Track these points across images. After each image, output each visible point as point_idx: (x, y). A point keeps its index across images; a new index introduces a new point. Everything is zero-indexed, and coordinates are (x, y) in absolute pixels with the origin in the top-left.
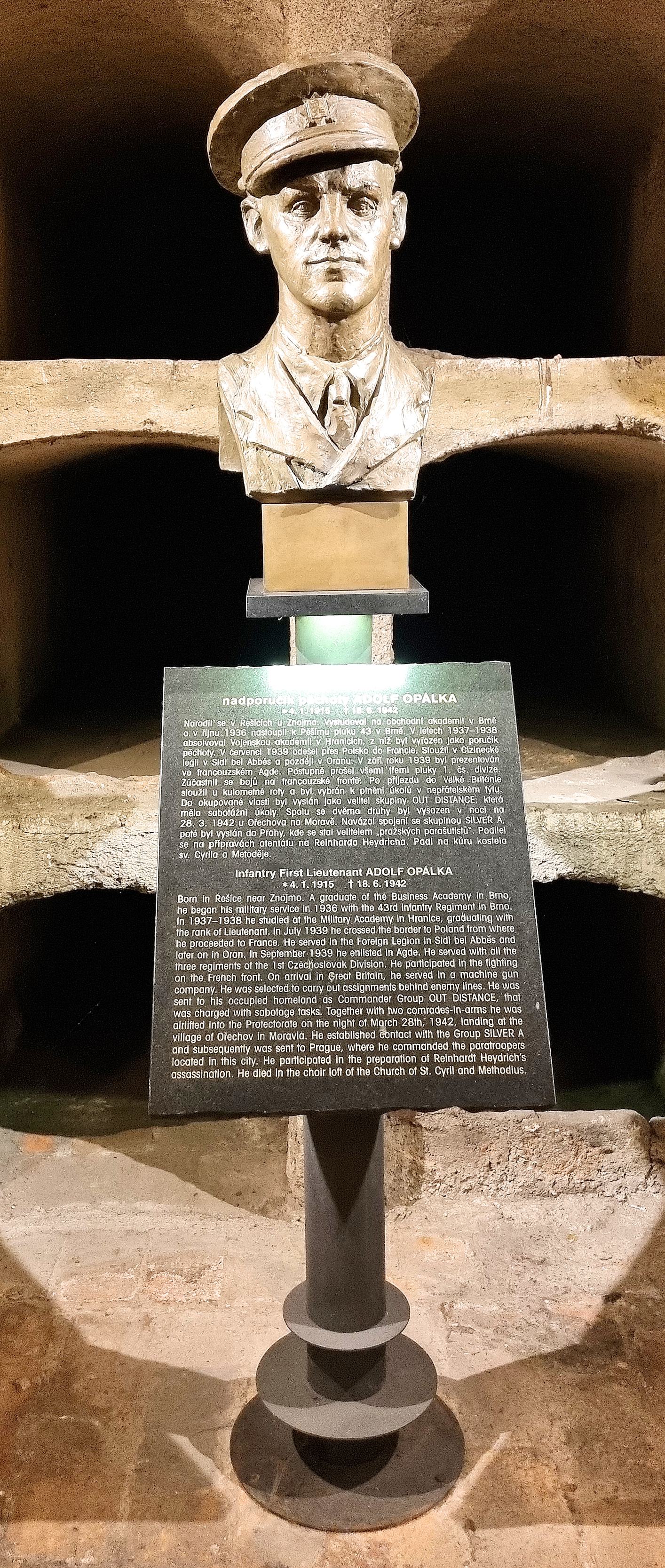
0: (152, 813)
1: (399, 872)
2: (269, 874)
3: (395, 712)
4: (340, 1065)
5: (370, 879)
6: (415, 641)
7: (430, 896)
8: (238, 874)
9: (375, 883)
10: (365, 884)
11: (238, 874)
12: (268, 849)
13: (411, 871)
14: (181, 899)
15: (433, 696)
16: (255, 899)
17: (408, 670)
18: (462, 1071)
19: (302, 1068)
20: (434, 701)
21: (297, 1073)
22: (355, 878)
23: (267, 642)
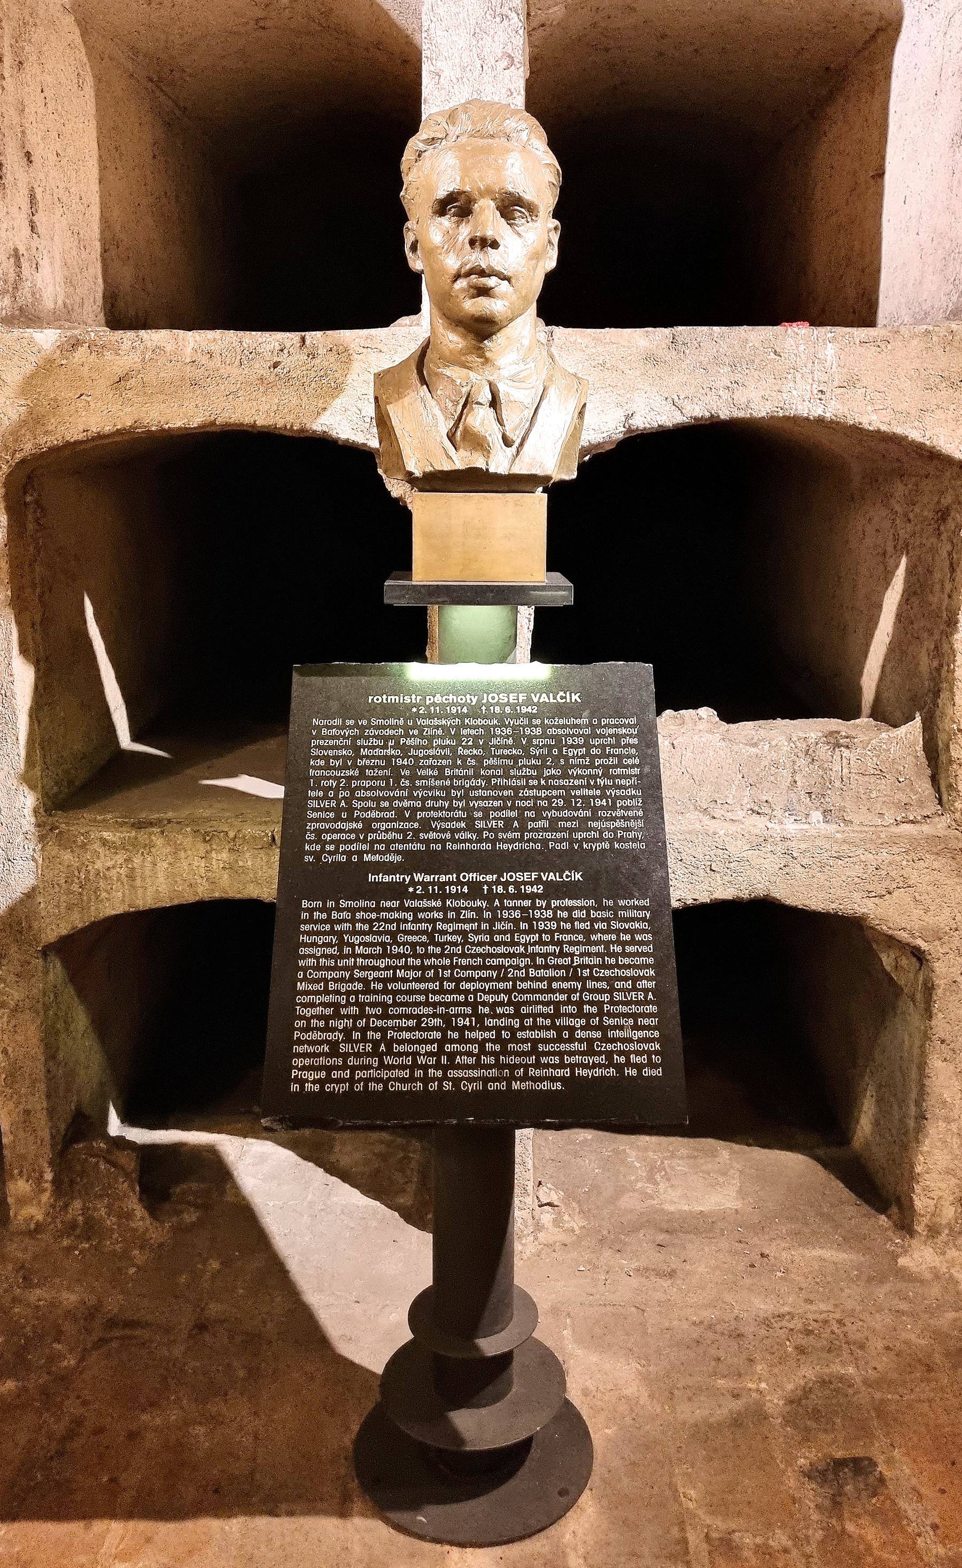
0: (693, 820)
1: (533, 877)
2: (404, 879)
3: (534, 711)
4: (420, 1080)
5: (506, 885)
6: (557, 638)
7: (325, 903)
8: (371, 878)
9: (511, 889)
10: (500, 889)
11: (371, 878)
12: (398, 852)
13: (464, 877)
14: (305, 904)
15: (551, 695)
16: (388, 904)
17: (543, 671)
18: (492, 1086)
19: (385, 1082)
20: (552, 700)
21: (380, 1087)
22: (490, 884)
23: (409, 636)
